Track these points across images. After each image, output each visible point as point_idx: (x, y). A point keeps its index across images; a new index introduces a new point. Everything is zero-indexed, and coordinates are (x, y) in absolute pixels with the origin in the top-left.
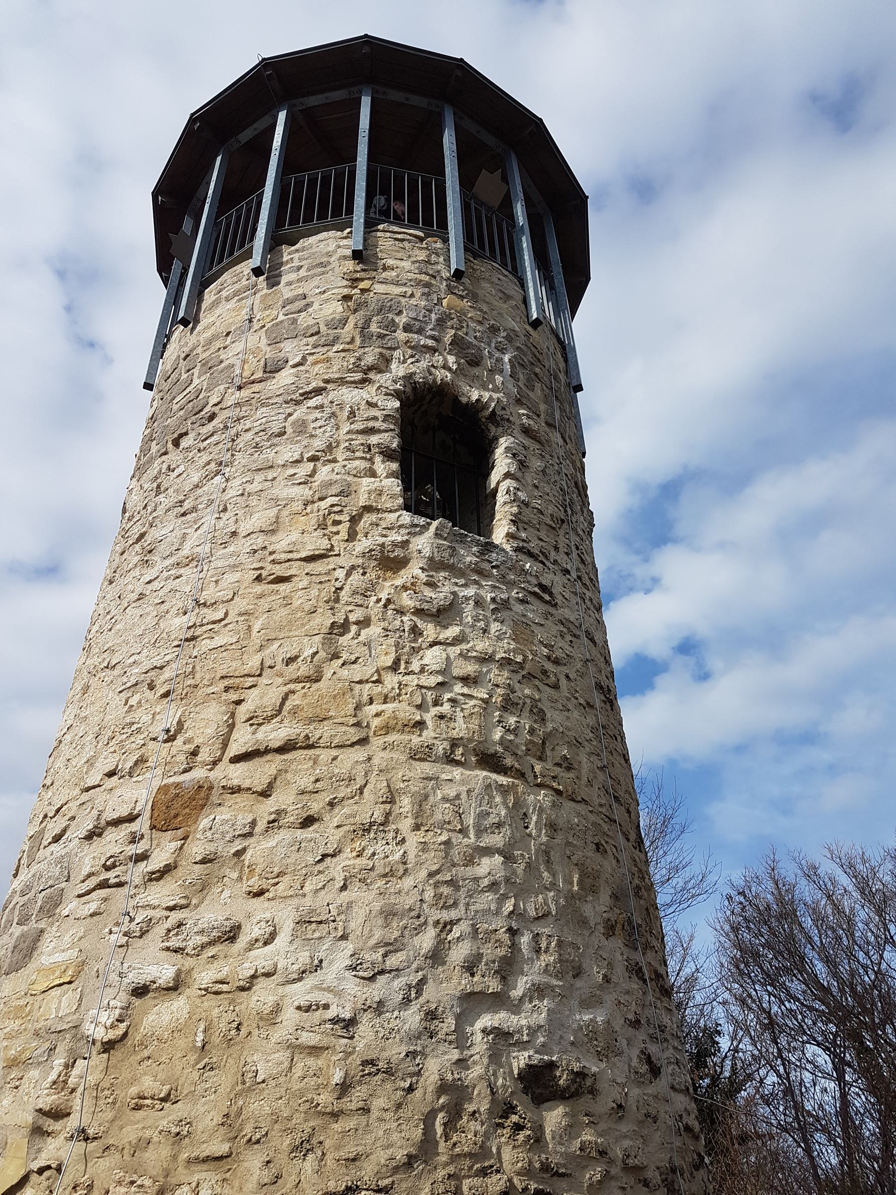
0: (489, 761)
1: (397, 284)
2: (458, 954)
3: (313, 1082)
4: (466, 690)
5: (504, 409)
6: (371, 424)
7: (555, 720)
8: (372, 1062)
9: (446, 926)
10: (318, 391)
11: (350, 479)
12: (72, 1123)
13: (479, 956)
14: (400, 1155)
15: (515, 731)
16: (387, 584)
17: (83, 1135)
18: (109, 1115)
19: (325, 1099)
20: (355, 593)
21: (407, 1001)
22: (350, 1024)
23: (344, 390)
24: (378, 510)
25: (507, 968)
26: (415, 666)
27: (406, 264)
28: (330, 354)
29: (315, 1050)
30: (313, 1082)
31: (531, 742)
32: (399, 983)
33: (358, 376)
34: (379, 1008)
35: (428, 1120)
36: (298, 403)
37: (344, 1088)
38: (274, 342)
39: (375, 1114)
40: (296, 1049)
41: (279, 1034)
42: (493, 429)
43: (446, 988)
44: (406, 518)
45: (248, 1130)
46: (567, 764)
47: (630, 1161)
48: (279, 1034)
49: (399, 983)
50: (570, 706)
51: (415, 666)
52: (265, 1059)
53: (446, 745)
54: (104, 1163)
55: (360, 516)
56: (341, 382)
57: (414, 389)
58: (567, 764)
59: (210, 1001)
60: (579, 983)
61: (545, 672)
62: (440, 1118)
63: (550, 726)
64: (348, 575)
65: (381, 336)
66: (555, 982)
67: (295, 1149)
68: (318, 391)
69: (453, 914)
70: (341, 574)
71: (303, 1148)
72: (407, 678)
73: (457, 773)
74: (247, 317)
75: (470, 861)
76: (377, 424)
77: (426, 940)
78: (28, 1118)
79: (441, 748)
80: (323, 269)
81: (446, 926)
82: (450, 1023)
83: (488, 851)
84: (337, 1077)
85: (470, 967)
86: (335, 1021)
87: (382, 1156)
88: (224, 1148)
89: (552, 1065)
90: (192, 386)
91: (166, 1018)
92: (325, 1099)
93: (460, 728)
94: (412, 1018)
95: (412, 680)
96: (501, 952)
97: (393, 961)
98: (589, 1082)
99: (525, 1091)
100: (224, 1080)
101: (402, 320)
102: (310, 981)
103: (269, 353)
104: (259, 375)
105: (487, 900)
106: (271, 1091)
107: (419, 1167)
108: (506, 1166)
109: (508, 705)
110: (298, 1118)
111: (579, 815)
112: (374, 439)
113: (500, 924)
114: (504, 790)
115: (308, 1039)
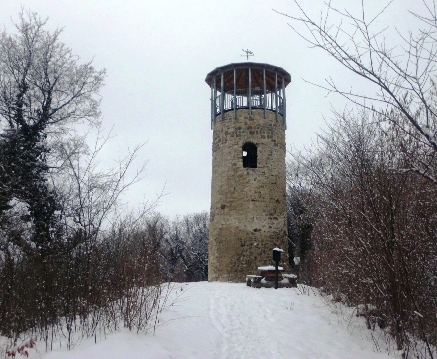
7: (262, 192)
56: (234, 145)
112: (239, 156)
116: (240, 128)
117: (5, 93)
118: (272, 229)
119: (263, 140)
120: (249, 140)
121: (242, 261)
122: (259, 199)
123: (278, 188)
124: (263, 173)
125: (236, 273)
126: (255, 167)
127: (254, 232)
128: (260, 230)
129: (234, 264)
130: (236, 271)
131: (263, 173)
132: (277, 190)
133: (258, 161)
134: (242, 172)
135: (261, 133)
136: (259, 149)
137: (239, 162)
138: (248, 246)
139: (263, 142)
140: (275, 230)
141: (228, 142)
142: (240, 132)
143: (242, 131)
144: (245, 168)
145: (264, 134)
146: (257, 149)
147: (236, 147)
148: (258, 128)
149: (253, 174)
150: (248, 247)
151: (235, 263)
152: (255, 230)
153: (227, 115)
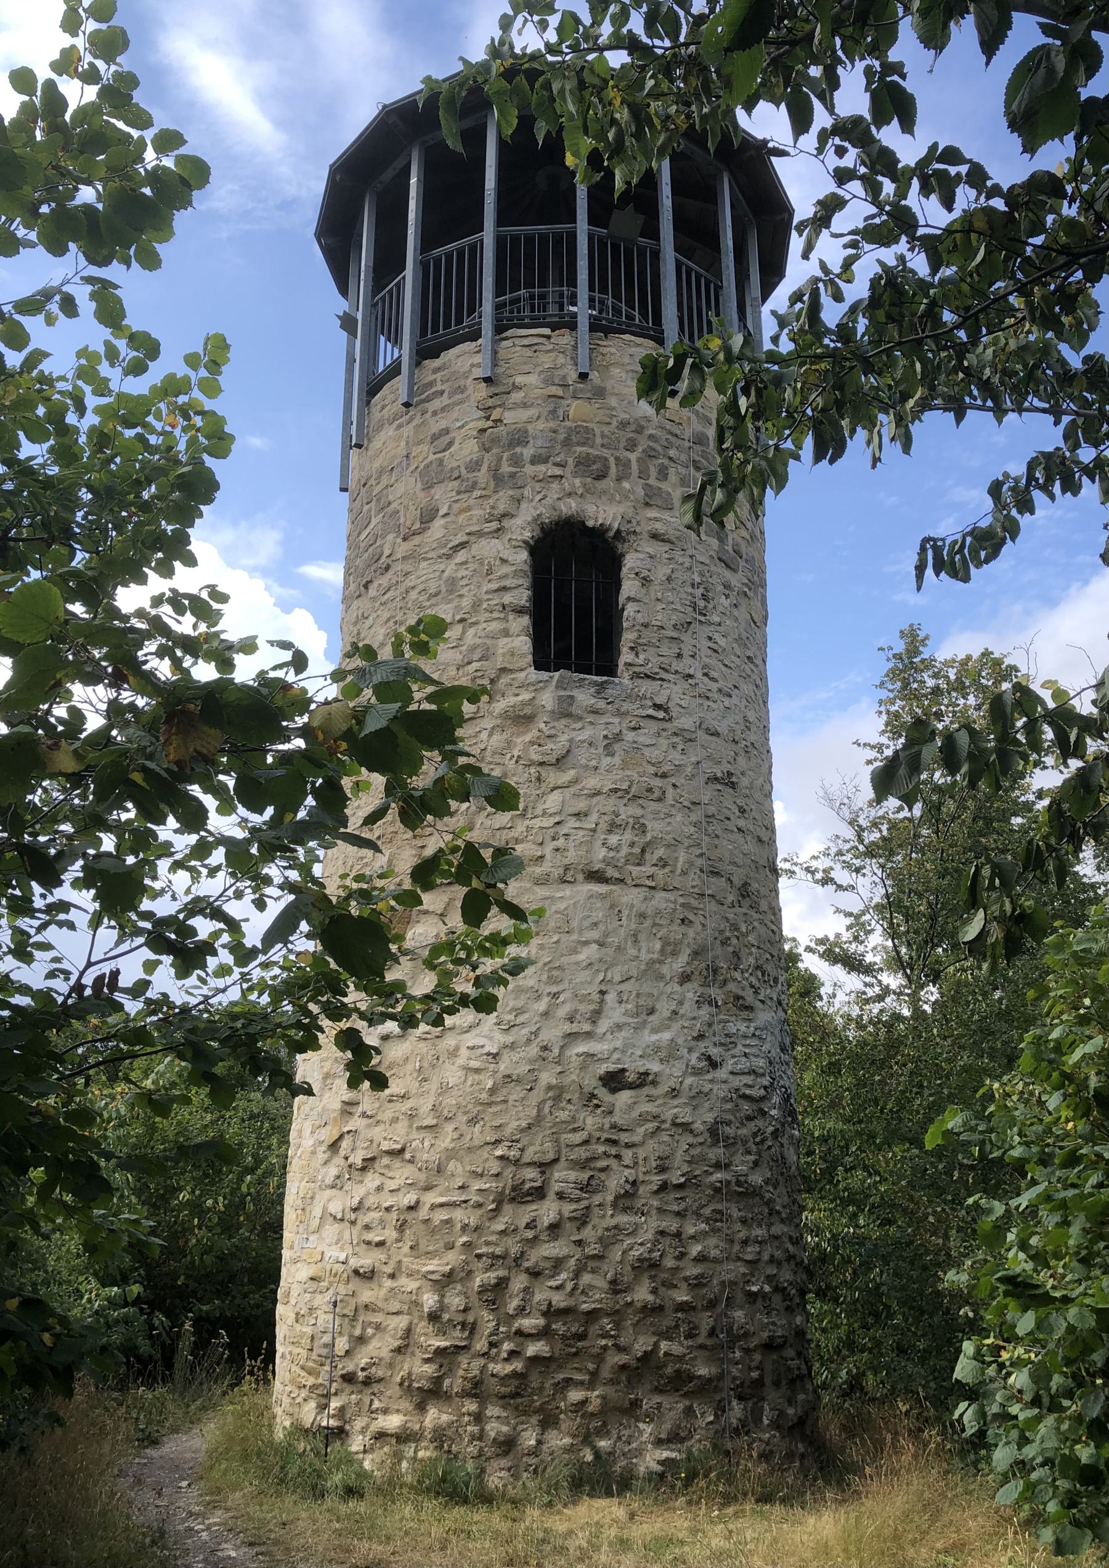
0: (595, 876)
1: (525, 405)
2: (563, 1012)
3: (477, 1088)
4: (578, 824)
5: (629, 522)
6: (503, 583)
7: (655, 828)
8: (509, 1076)
9: (555, 996)
10: (463, 545)
11: (488, 642)
12: (360, 1109)
13: (576, 1011)
14: (524, 1124)
15: (617, 849)
16: (519, 740)
17: (364, 1115)
18: (377, 1105)
19: (484, 1096)
20: (494, 753)
21: (529, 1041)
22: (495, 1056)
23: (483, 542)
24: (511, 671)
25: (595, 1016)
26: (539, 811)
27: (533, 379)
28: (471, 502)
29: (477, 1071)
30: (477, 1088)
31: (631, 854)
32: (525, 1031)
33: (494, 525)
34: (512, 1046)
35: (540, 1107)
36: (449, 557)
37: (493, 1091)
38: (428, 487)
39: (511, 1103)
40: (468, 1070)
41: (461, 1061)
42: (620, 546)
43: (553, 1033)
44: (533, 674)
45: (445, 1112)
46: (662, 863)
47: (679, 1121)
48: (461, 1061)
49: (525, 1031)
50: (674, 812)
51: (539, 811)
52: (452, 1074)
53: (561, 871)
54: (378, 1129)
55: (498, 677)
56: (480, 534)
57: (542, 529)
58: (662, 863)
59: (422, 1044)
60: (651, 1018)
61: (650, 790)
62: (549, 1103)
63: (649, 837)
64: (490, 735)
65: (512, 476)
66: (631, 1020)
67: (469, 1121)
68: (463, 545)
69: (560, 988)
70: (484, 736)
71: (473, 1121)
72: (533, 821)
73: (567, 891)
74: (405, 453)
75: (574, 951)
76: (508, 583)
77: (542, 1006)
78: (338, 1106)
79: (557, 872)
80: (460, 396)
81: (555, 996)
82: (556, 1051)
83: (586, 943)
84: (490, 1084)
85: (571, 1019)
86: (488, 1054)
87: (514, 1124)
88: (434, 1122)
89: (624, 1070)
90: (371, 526)
91: (400, 1053)
92: (484, 1096)
93: (572, 856)
94: (533, 1050)
95: (537, 823)
96: (592, 1007)
97: (521, 1019)
98: (651, 1078)
99: (604, 1085)
100: (433, 1086)
101: (527, 452)
102: (474, 1032)
103: (423, 499)
104: (417, 525)
105: (584, 976)
106: (455, 1092)
107: (534, 1130)
108: (588, 1127)
109: (613, 827)
110: (470, 1106)
111: (668, 901)
112: (507, 599)
113: (594, 989)
114: (603, 897)
115: (474, 1064)
116: (520, 438)
117: (503, 1397)
118: (722, 1074)
119: (654, 518)
120: (570, 507)
121: (521, 1311)
122: (636, 870)
123: (742, 811)
124: (657, 707)
125: (472, 1406)
126: (608, 668)
127: (602, 1093)
128: (644, 1080)
129: (456, 1337)
130: (476, 1389)
131: (657, 707)
132: (741, 823)
133: (628, 637)
134: (526, 696)
135: (643, 474)
136: (631, 562)
137: (506, 633)
138: (561, 1196)
139: (659, 527)
140: (737, 1082)
141: (439, 523)
142: (516, 461)
143: (527, 452)
144: (544, 675)
145: (664, 486)
146: (616, 562)
147: (489, 548)
148: (631, 446)
149: (596, 712)
150: (568, 1208)
151: (471, 1329)
152: (614, 1081)
153: (437, 370)
